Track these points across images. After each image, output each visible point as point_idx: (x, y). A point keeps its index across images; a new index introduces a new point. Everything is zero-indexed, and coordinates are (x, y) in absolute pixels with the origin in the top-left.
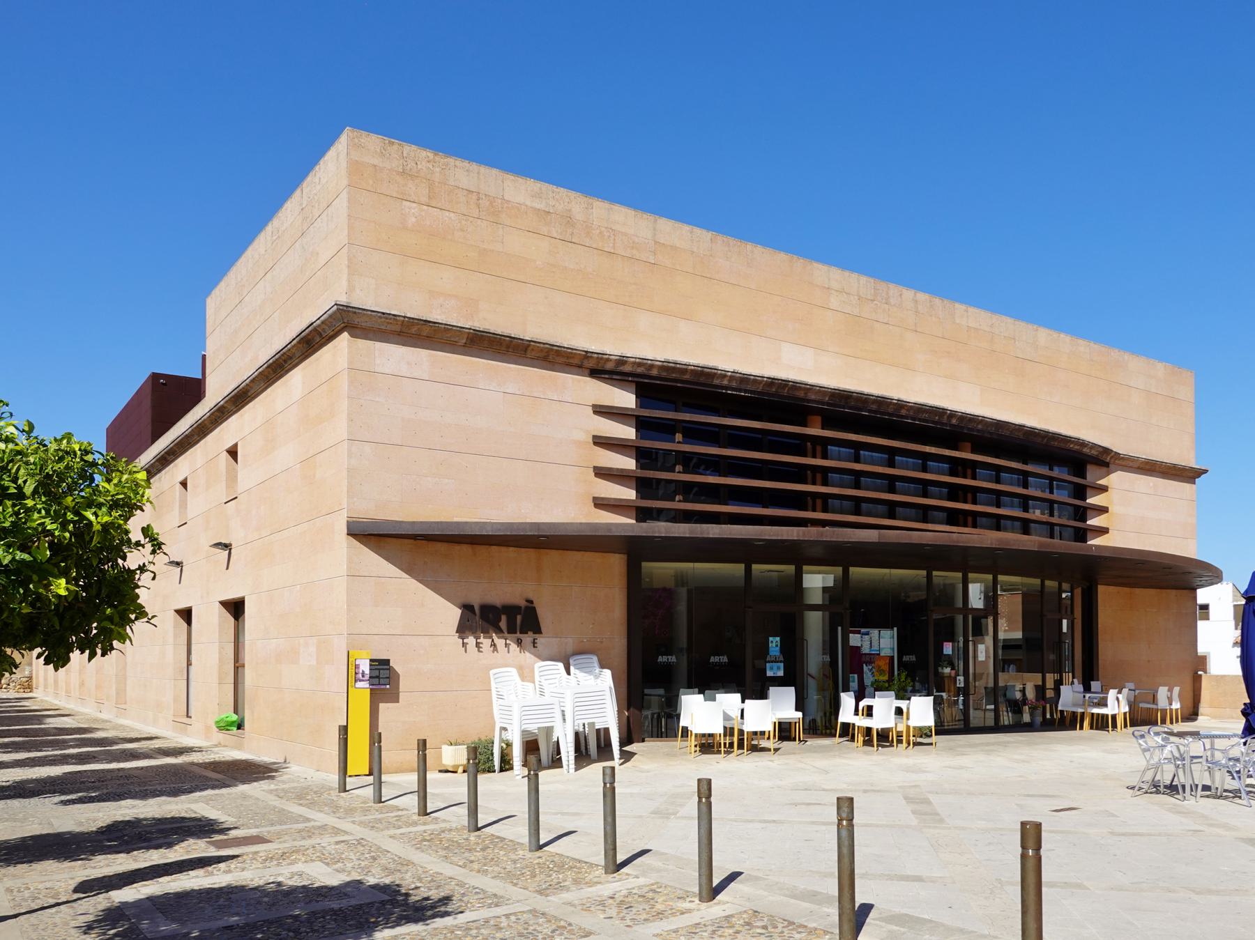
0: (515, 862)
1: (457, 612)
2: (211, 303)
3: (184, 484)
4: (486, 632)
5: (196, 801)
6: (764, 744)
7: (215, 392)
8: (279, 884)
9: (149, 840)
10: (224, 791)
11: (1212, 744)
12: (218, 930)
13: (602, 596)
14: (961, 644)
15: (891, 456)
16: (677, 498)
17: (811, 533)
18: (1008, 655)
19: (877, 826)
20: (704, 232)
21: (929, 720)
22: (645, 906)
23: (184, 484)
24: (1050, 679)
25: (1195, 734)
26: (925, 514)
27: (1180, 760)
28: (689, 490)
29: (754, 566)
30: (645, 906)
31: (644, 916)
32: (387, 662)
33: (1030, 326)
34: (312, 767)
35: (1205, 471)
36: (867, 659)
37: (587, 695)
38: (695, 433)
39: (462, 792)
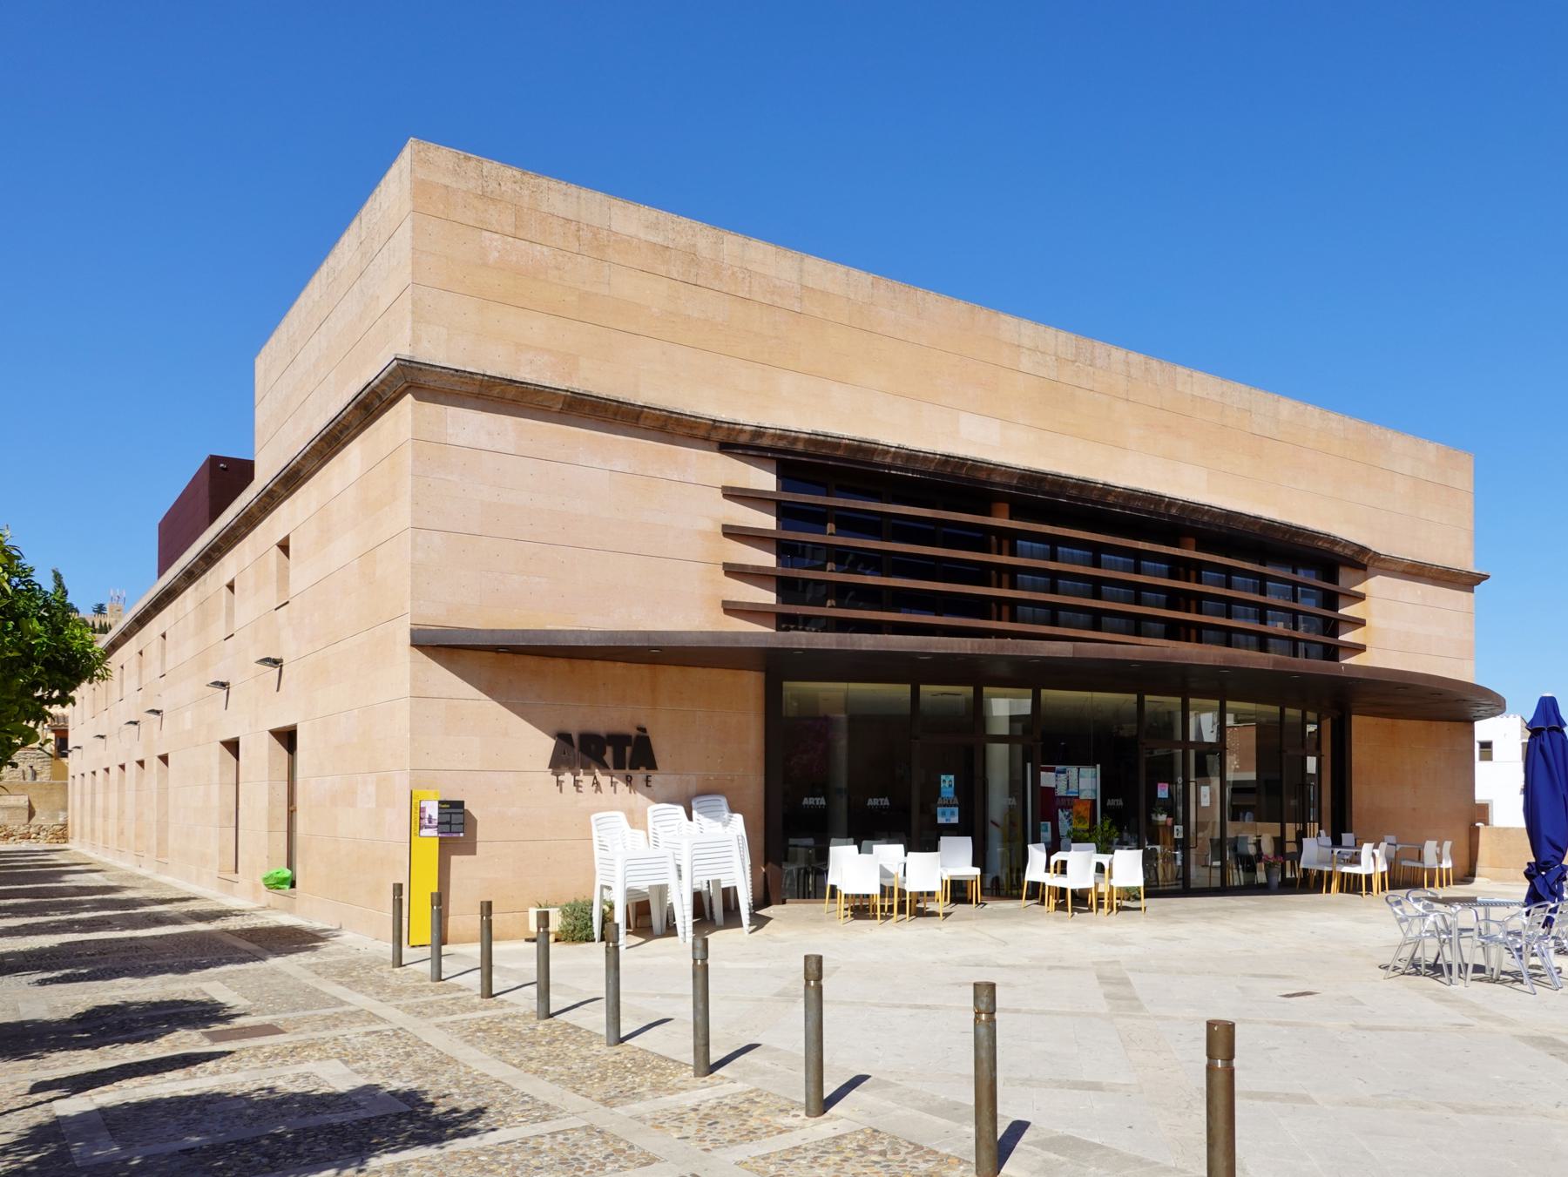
0: (585, 1059)
1: (550, 743)
2: (260, 364)
3: (231, 587)
4: (586, 767)
5: (211, 979)
6: (931, 907)
7: (264, 476)
8: (271, 1090)
9: (131, 1031)
10: (250, 965)
11: (1487, 914)
12: (172, 1155)
13: (734, 722)
14: (1180, 787)
15: (1096, 553)
16: (829, 603)
17: (989, 646)
18: (1240, 801)
19: (1058, 1014)
20: (863, 274)
21: (1137, 880)
22: (736, 1121)
23: (231, 587)
24: (1291, 830)
25: (1470, 901)
26: (1137, 626)
27: (1446, 933)
28: (842, 593)
29: (923, 688)
30: (736, 1121)
31: (730, 1136)
32: (460, 804)
33: (1270, 395)
34: (363, 936)
35: (1486, 577)
36: (1063, 802)
37: (710, 846)
38: (851, 523)
39: (530, 967)
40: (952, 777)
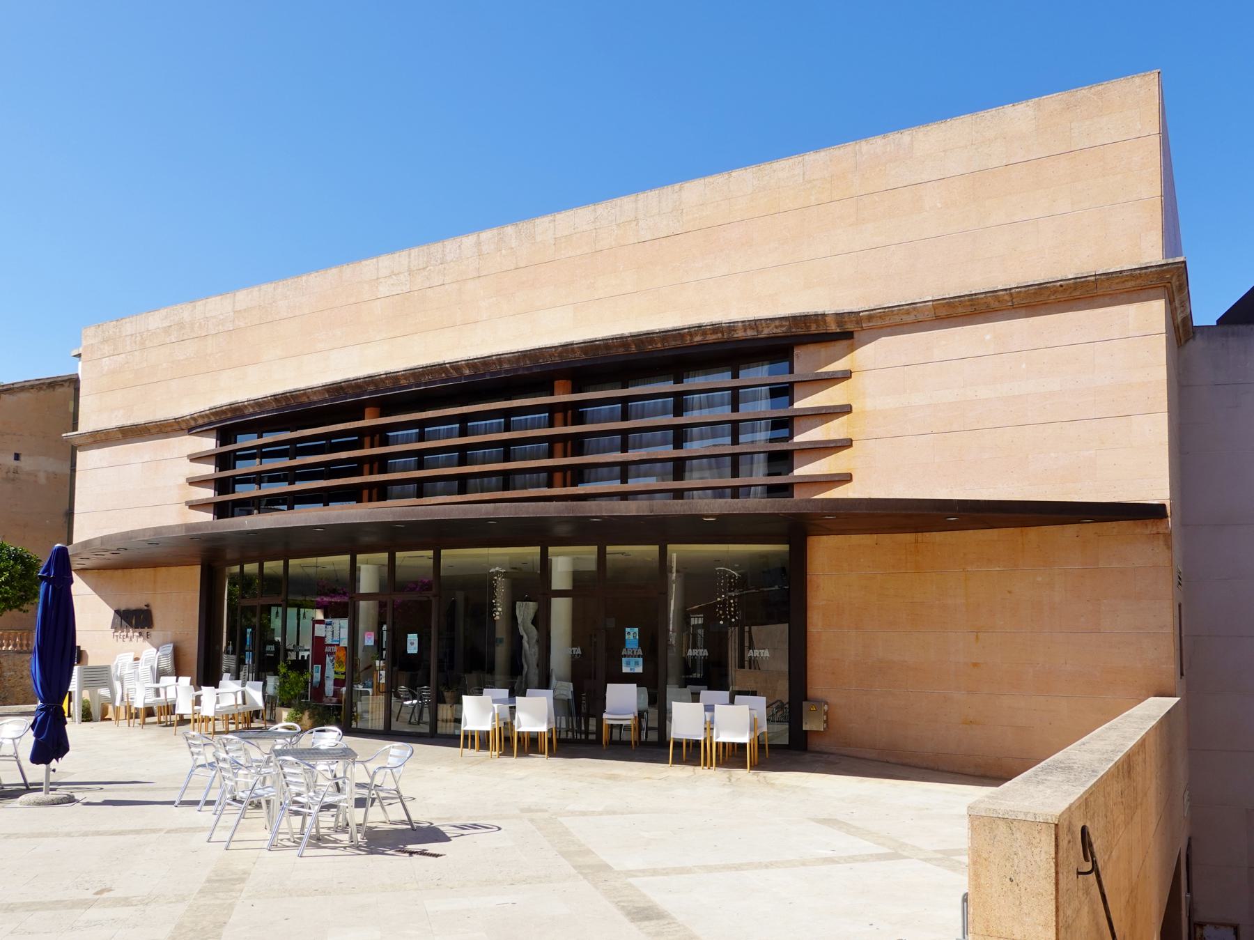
40: (636, 630)
